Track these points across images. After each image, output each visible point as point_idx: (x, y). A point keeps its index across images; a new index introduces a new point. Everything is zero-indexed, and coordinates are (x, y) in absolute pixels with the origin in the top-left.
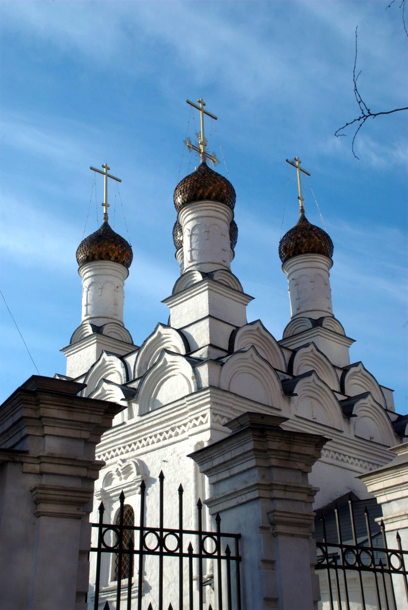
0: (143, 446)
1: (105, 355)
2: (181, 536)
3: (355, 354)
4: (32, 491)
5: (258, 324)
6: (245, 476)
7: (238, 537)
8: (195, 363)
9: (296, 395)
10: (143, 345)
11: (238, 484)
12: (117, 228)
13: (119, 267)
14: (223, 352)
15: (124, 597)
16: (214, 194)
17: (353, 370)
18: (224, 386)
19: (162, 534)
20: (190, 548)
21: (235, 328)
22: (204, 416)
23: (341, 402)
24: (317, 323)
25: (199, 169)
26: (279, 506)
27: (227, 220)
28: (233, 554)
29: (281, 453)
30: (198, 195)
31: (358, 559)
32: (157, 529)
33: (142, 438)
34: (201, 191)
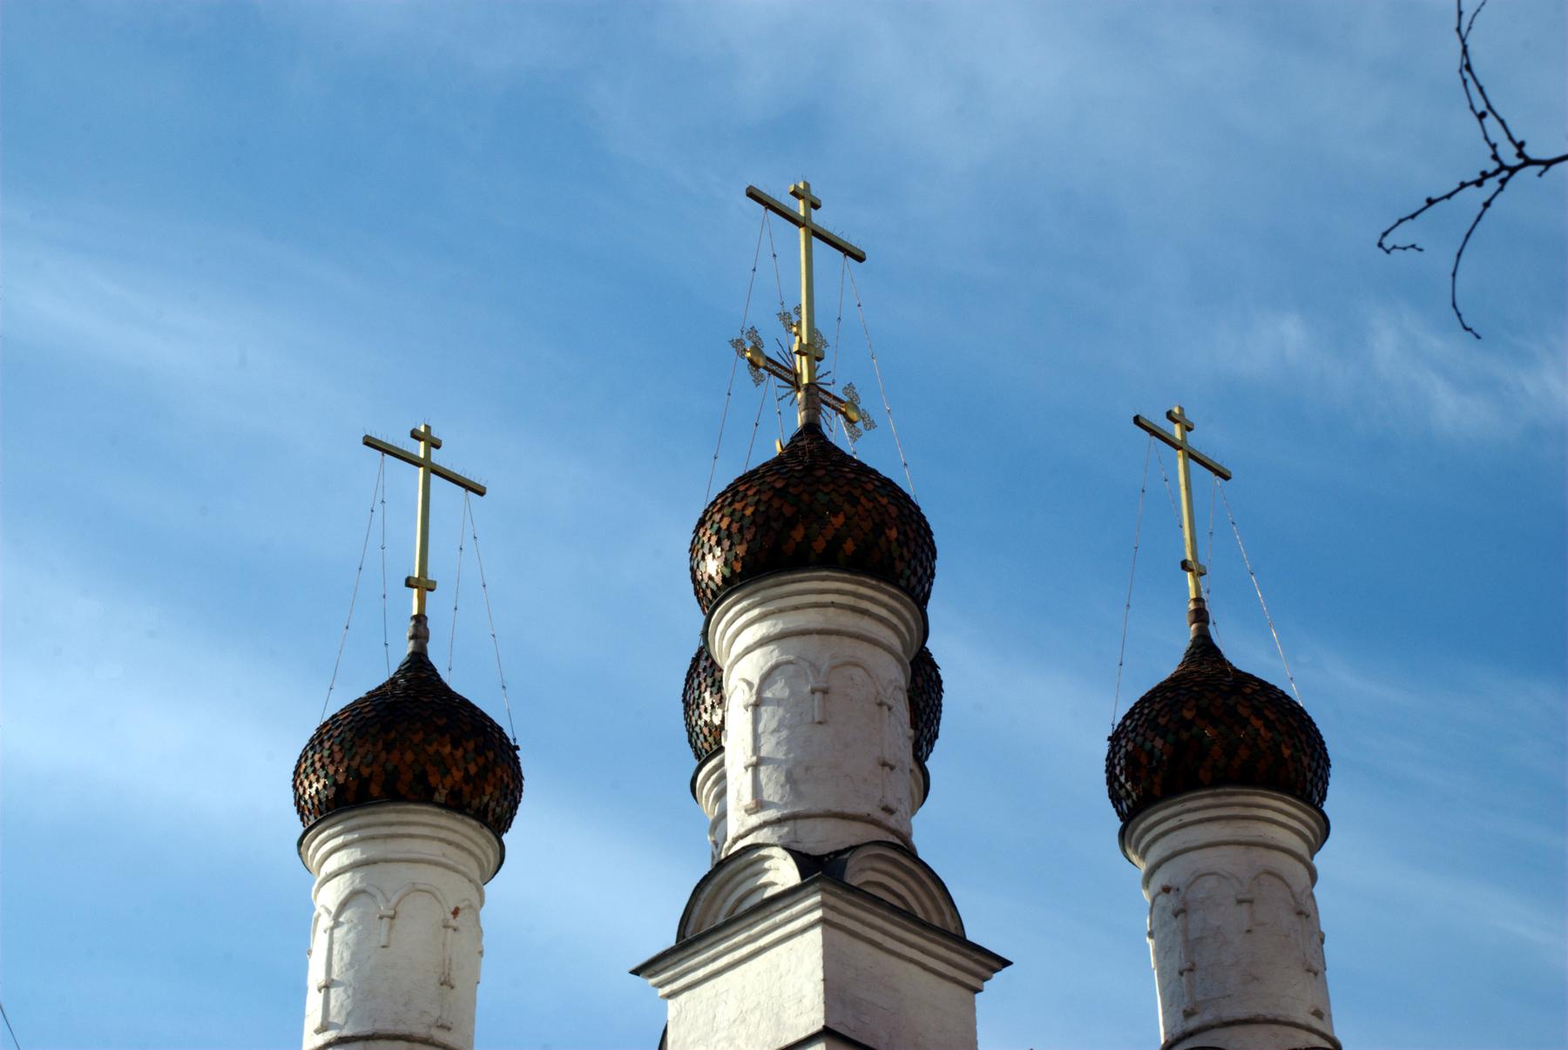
12: (461, 674)
13: (464, 830)
16: (849, 546)
25: (792, 449)
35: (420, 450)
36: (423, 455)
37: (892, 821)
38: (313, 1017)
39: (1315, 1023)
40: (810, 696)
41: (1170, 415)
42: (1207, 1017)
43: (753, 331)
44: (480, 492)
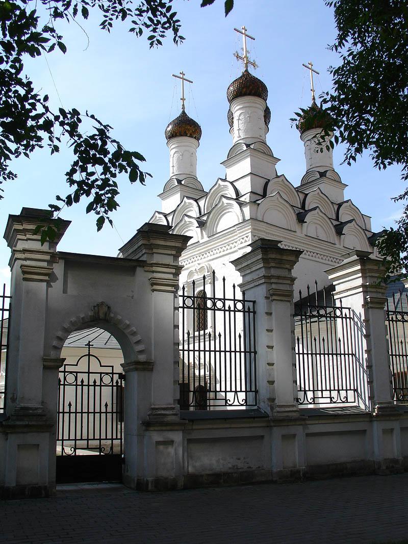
0: (211, 255)
1: (185, 198)
2: (224, 301)
3: (347, 195)
4: (149, 280)
5: (282, 177)
6: (258, 272)
7: (254, 302)
8: (241, 205)
9: (306, 222)
10: (210, 192)
11: (255, 276)
12: (191, 115)
13: (193, 140)
14: (260, 194)
15: (202, 340)
16: (253, 92)
17: (345, 205)
18: (260, 218)
19: (214, 301)
20: (229, 307)
21: (267, 181)
22: (247, 237)
23: (335, 226)
24: (323, 175)
25: (243, 75)
26: (274, 286)
27: (262, 109)
28: (252, 310)
29: (277, 260)
30: (243, 93)
31: (318, 312)
32: (237, 311)
33: (245, 236)
34: (244, 90)
35: (181, 76)
36: (182, 77)
37: (261, 138)
38: (171, 171)
39: (330, 166)
40: (250, 121)
41: (309, 64)
42: (314, 166)
43: (237, 52)
44: (192, 82)
